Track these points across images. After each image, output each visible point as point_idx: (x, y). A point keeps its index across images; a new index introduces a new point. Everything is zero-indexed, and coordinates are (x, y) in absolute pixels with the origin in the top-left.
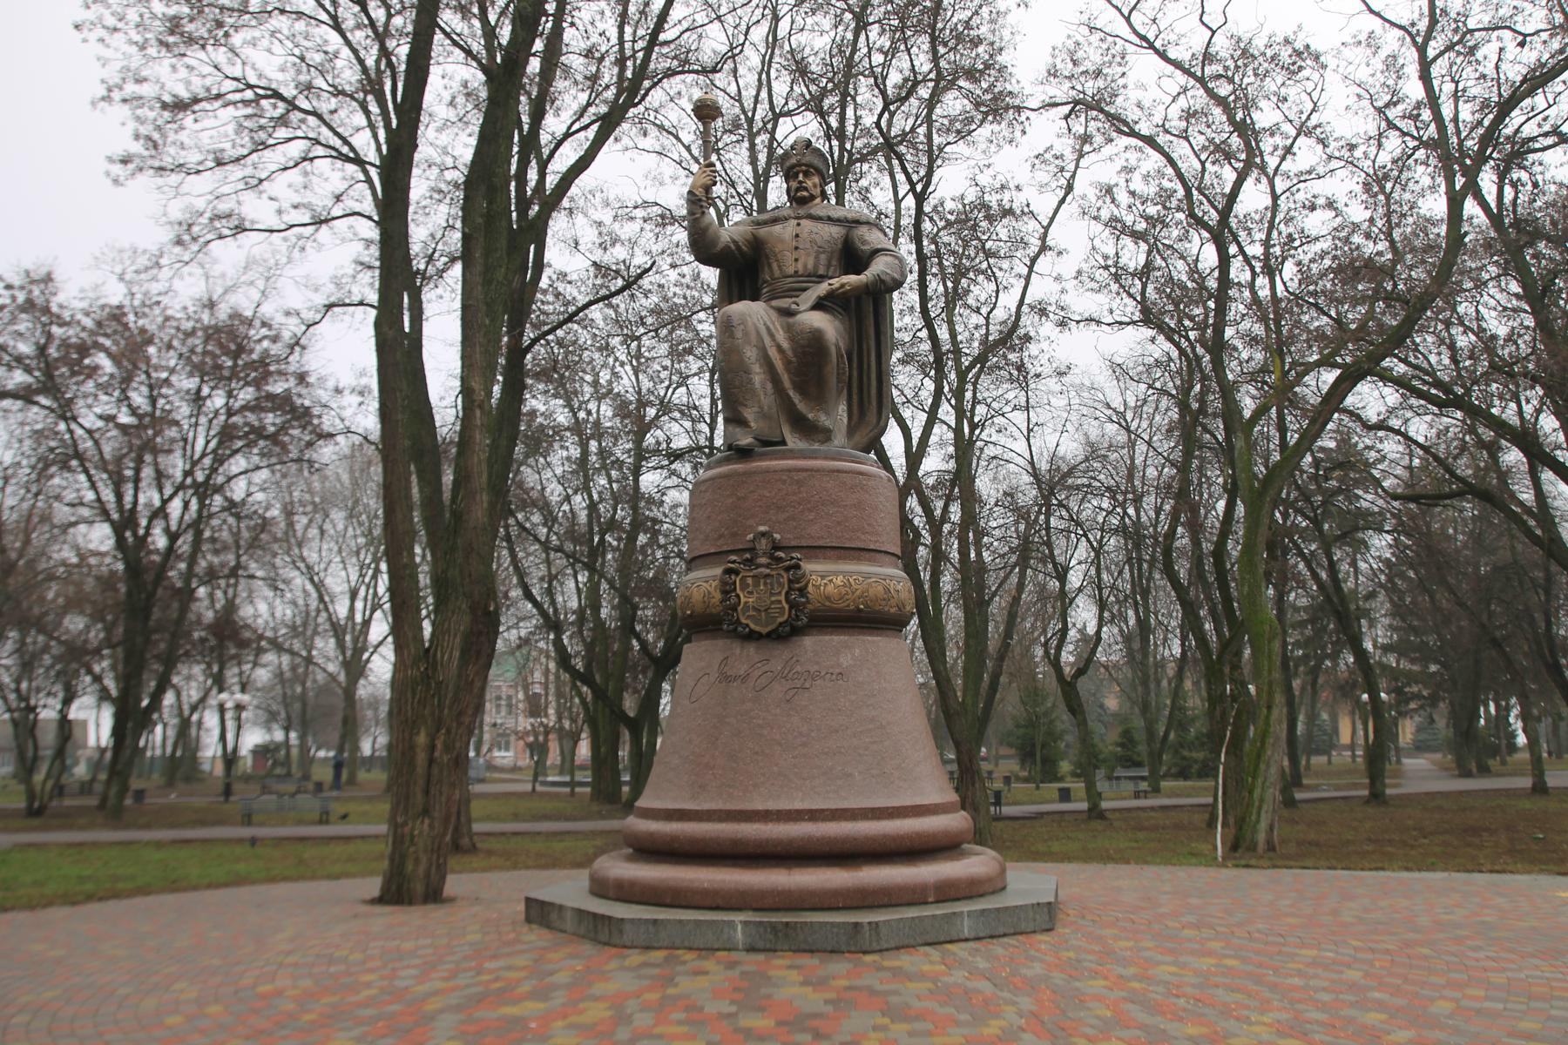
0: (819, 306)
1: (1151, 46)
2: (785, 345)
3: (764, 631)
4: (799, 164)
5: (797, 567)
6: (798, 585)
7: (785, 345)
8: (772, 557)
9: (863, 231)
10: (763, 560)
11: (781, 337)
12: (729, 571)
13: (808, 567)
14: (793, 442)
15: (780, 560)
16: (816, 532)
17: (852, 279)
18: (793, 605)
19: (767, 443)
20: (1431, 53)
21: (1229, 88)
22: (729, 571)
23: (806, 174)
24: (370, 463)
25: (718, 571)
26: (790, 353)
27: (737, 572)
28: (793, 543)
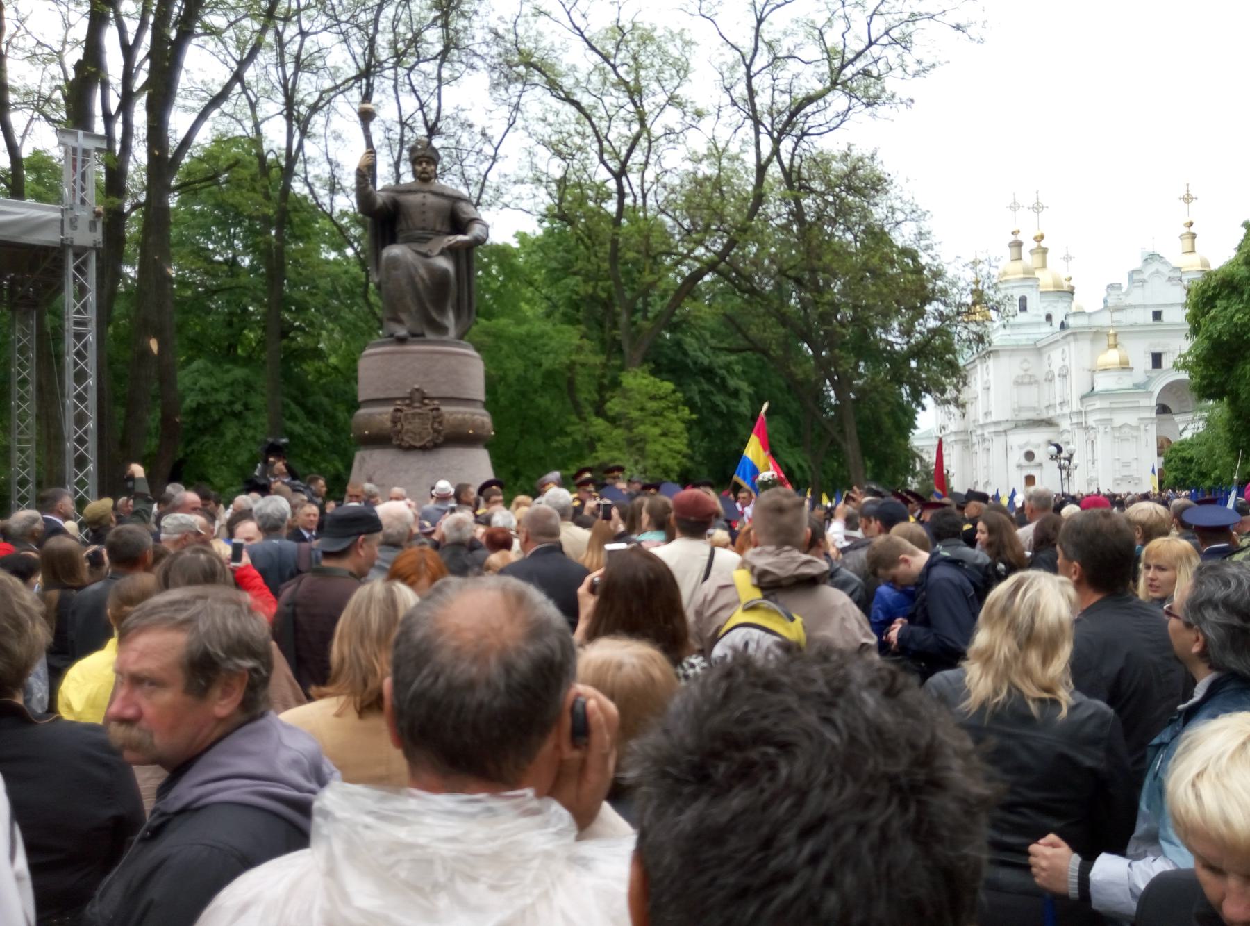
0: (442, 253)
1: (582, 34)
2: (425, 276)
3: (418, 444)
4: (423, 156)
5: (438, 409)
6: (438, 417)
7: (425, 276)
8: (422, 402)
9: (463, 205)
10: (417, 404)
11: (422, 271)
12: (397, 410)
13: (444, 409)
14: (430, 336)
15: (426, 405)
16: (447, 391)
17: (461, 238)
18: (436, 431)
19: (414, 335)
20: (754, 69)
21: (631, 61)
22: (397, 410)
23: (428, 163)
24: (224, 114)
25: (391, 409)
26: (428, 282)
27: (401, 411)
28: (434, 395)
